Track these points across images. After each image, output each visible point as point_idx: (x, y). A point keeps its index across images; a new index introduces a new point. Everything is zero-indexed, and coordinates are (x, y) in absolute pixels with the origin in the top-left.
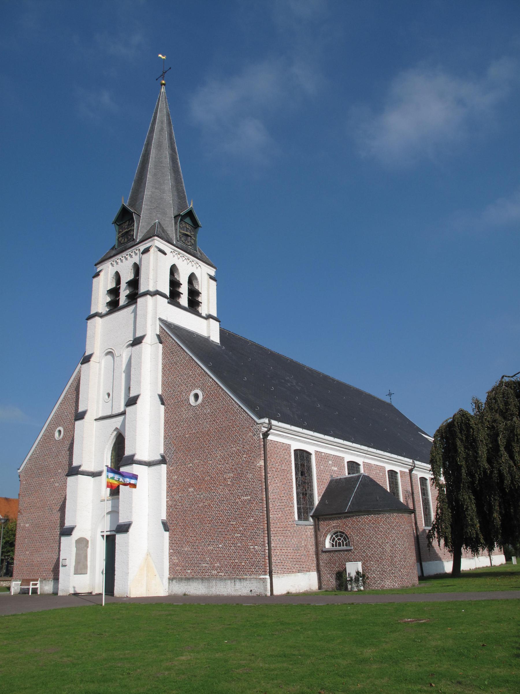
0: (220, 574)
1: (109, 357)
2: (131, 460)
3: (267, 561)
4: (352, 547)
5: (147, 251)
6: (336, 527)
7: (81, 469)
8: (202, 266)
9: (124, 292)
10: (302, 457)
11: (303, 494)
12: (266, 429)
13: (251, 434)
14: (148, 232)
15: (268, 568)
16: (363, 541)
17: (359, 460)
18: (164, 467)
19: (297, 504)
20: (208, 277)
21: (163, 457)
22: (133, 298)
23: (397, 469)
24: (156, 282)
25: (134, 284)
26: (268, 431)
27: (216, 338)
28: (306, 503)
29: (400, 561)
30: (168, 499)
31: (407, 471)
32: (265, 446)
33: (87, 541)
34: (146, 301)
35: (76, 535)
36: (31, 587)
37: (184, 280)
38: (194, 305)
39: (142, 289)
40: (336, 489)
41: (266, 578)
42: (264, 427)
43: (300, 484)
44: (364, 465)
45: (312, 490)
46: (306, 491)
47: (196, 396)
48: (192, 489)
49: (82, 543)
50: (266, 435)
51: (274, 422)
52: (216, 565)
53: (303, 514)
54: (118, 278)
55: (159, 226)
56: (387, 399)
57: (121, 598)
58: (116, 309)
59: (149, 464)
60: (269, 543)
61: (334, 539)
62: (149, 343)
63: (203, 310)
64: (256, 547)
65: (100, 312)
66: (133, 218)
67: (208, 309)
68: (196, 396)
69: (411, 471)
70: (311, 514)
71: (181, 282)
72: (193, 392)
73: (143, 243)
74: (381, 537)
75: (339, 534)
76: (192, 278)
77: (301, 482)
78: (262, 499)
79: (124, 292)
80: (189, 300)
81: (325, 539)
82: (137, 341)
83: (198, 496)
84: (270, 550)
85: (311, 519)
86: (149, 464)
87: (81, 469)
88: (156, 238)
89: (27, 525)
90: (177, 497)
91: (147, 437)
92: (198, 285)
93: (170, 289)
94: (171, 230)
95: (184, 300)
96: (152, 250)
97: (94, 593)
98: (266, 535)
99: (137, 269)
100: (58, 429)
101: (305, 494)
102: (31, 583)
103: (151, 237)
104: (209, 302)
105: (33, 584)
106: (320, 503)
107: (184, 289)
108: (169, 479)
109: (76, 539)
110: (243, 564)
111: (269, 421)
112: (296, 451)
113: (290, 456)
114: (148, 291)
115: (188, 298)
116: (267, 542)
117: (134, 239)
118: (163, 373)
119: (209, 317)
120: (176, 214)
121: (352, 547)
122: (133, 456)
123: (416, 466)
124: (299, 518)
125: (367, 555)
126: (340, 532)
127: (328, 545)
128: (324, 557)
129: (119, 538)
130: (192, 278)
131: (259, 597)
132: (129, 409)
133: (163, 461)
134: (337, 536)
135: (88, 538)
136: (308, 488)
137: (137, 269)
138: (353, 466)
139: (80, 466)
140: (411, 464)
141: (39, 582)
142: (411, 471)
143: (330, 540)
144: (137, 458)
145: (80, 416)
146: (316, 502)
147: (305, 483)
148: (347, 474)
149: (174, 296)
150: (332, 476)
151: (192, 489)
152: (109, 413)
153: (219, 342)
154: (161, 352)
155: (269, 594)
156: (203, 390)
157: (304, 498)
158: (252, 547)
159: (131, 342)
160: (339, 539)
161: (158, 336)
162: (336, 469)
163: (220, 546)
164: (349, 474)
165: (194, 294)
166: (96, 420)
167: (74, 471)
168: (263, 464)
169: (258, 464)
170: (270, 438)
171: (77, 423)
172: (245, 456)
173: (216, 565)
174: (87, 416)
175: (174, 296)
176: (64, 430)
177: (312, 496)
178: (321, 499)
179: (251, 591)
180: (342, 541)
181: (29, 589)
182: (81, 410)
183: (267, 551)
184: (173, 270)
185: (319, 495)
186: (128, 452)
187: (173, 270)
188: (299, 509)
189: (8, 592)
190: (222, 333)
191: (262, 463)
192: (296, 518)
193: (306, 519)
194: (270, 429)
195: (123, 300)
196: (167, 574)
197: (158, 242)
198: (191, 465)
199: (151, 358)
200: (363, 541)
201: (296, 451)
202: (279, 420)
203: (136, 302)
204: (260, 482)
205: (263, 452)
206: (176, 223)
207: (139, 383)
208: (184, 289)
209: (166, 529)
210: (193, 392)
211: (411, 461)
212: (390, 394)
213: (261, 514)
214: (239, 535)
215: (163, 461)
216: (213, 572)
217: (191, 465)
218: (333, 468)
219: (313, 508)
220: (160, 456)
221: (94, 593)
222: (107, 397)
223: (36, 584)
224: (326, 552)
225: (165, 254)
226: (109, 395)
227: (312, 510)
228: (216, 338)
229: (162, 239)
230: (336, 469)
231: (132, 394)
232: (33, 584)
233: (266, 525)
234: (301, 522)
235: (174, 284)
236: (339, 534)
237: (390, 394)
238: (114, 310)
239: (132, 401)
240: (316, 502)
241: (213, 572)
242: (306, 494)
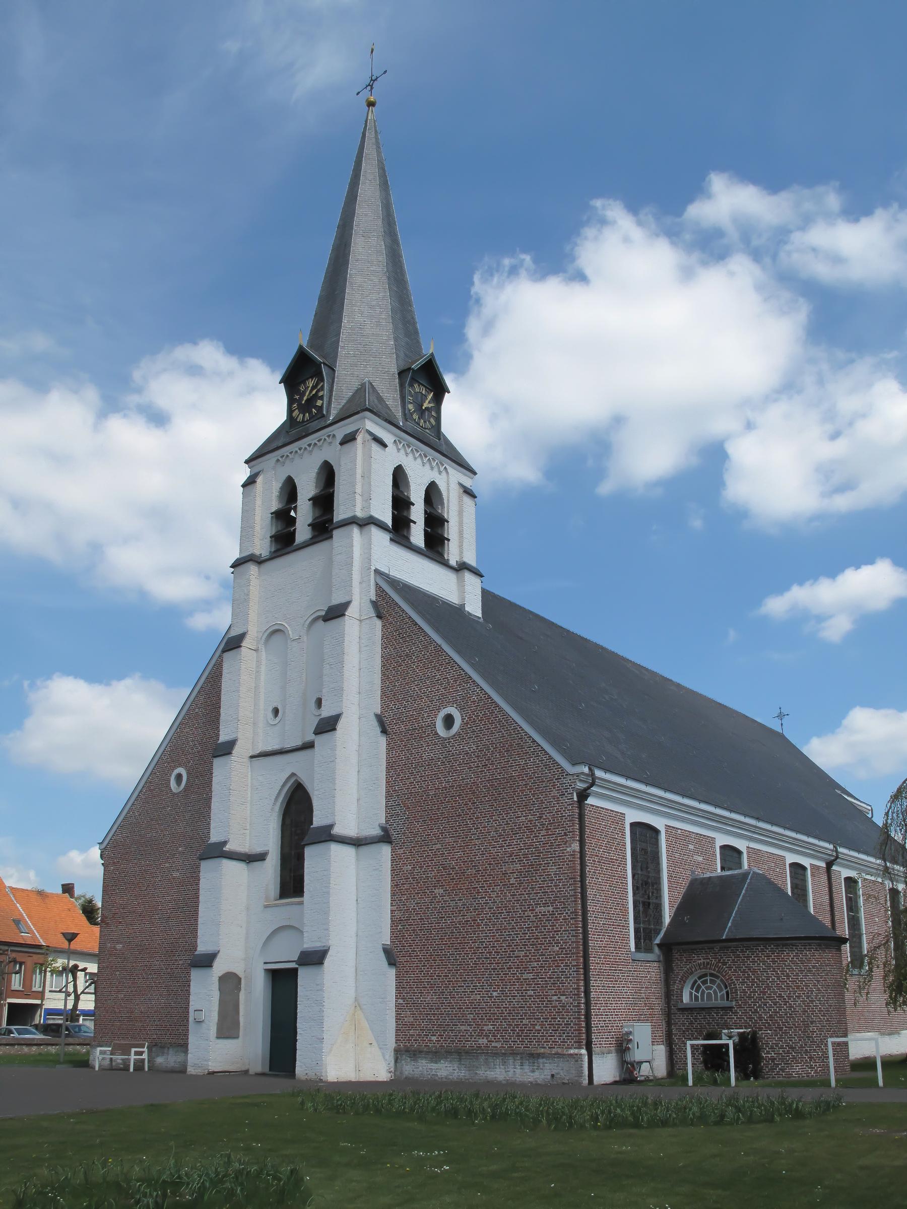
0: (493, 1044)
1: (277, 638)
2: (327, 835)
3: (583, 1024)
4: (734, 1003)
5: (349, 439)
6: (705, 966)
7: (227, 848)
8: (450, 470)
9: (304, 514)
10: (645, 835)
11: (644, 903)
12: (585, 786)
13: (555, 793)
14: (350, 400)
15: (584, 1036)
16: (755, 992)
17: (741, 845)
18: (386, 851)
19: (635, 923)
20: (462, 491)
21: (384, 829)
22: (324, 528)
23: (806, 862)
24: (368, 499)
25: (324, 501)
26: (589, 788)
27: (474, 608)
28: (649, 921)
29: (821, 1030)
30: (394, 908)
31: (823, 865)
32: (581, 817)
33: (239, 979)
34: (351, 538)
35: (220, 967)
36: (133, 1057)
37: (417, 496)
38: (435, 544)
39: (340, 513)
40: (703, 898)
41: (581, 1054)
42: (581, 781)
43: (639, 885)
44: (748, 852)
45: (659, 896)
46: (649, 898)
47: (449, 721)
48: (441, 891)
49: (231, 983)
50: (583, 795)
51: (599, 773)
52: (485, 1028)
53: (644, 938)
54: (290, 491)
55: (371, 391)
56: (775, 725)
57: (308, 1081)
58: (289, 549)
59: (357, 843)
60: (587, 993)
61: (699, 987)
62: (357, 616)
63: (453, 554)
64: (563, 998)
65: (257, 552)
66: (321, 373)
67: (461, 552)
68: (449, 721)
69: (829, 865)
70: (657, 941)
71: (412, 500)
72: (442, 714)
73: (342, 423)
74: (788, 987)
75: (699, 982)
76: (432, 493)
77: (640, 882)
78: (575, 912)
79: (304, 514)
80: (427, 535)
81: (682, 988)
82: (336, 613)
83: (452, 904)
84: (588, 1004)
85: (656, 950)
86: (357, 843)
87: (227, 848)
88: (368, 414)
89: (119, 946)
90: (412, 905)
91: (353, 786)
92: (443, 507)
93: (393, 513)
94: (391, 396)
95: (417, 535)
96: (360, 438)
97: (251, 1072)
98: (582, 977)
99: (328, 474)
100: (176, 771)
101: (647, 905)
102: (133, 1050)
103: (357, 413)
104: (461, 543)
105: (137, 1053)
106: (670, 924)
107: (417, 513)
108: (395, 871)
109: (220, 974)
110: (537, 1027)
111: (590, 769)
112: (632, 825)
113: (624, 834)
114: (355, 517)
115: (425, 530)
116: (582, 989)
117: (323, 416)
118: (383, 674)
119: (462, 567)
120: (402, 368)
121: (734, 1003)
122: (331, 826)
123: (840, 856)
124: (219, 1037)
125: (760, 1018)
126: (712, 975)
127: (686, 999)
128: (681, 1019)
129: (305, 976)
130: (432, 493)
131: (574, 1085)
132: (319, 740)
133: (385, 838)
134: (704, 982)
135: (241, 974)
136: (653, 893)
137: (328, 474)
138: (731, 854)
139: (225, 843)
140: (830, 852)
141: (145, 1049)
142: (829, 865)
143: (692, 988)
144: (336, 830)
145: (227, 749)
146: (667, 920)
147: (646, 883)
148: (719, 870)
149: (399, 528)
150: (693, 872)
151: (441, 891)
152: (276, 747)
153: (480, 616)
154: (379, 634)
155: (586, 1082)
156: (461, 709)
157: (645, 912)
158: (555, 998)
159: (323, 613)
160: (710, 988)
161: (374, 604)
162: (700, 859)
163: (495, 994)
164: (723, 869)
165: (435, 524)
166: (252, 757)
167: (218, 852)
168: (578, 849)
169: (568, 849)
170: (590, 801)
171: (217, 762)
172: (543, 832)
173: (485, 1028)
174: (236, 750)
175: (399, 528)
176: (188, 774)
177: (659, 907)
178: (675, 914)
179: (553, 1076)
180: (715, 992)
181: (129, 1060)
182: (223, 738)
183: (583, 1006)
184: (399, 477)
185: (671, 906)
186: (318, 820)
187: (399, 477)
188: (637, 931)
189: (180, 1058)
190: (487, 596)
191: (576, 846)
192: (633, 949)
193: (649, 950)
194: (593, 784)
195: (303, 532)
196: (391, 1043)
197: (372, 425)
198: (438, 846)
199: (360, 644)
200: (755, 992)
201: (633, 825)
202: (606, 770)
203: (331, 537)
204: (571, 882)
205: (577, 826)
206: (402, 385)
207: (339, 691)
208: (417, 513)
209: (392, 963)
210: (442, 714)
211: (831, 847)
212: (781, 716)
213: (574, 939)
214: (531, 976)
215: (385, 838)
216: (481, 1041)
217: (438, 846)
218: (695, 857)
219: (660, 930)
220: (378, 828)
221: (251, 1072)
222: (270, 715)
223: (141, 1053)
224: (684, 1010)
225: (384, 445)
226: (276, 712)
227: (658, 934)
228: (474, 608)
229: (379, 416)
230: (700, 859)
231: (327, 711)
232: (137, 1053)
233: (582, 960)
234: (641, 956)
235: (401, 504)
236: (699, 982)
237: (781, 716)
238: (284, 551)
239: (328, 726)
240: (667, 920)
241: (481, 1041)
242: (649, 904)
